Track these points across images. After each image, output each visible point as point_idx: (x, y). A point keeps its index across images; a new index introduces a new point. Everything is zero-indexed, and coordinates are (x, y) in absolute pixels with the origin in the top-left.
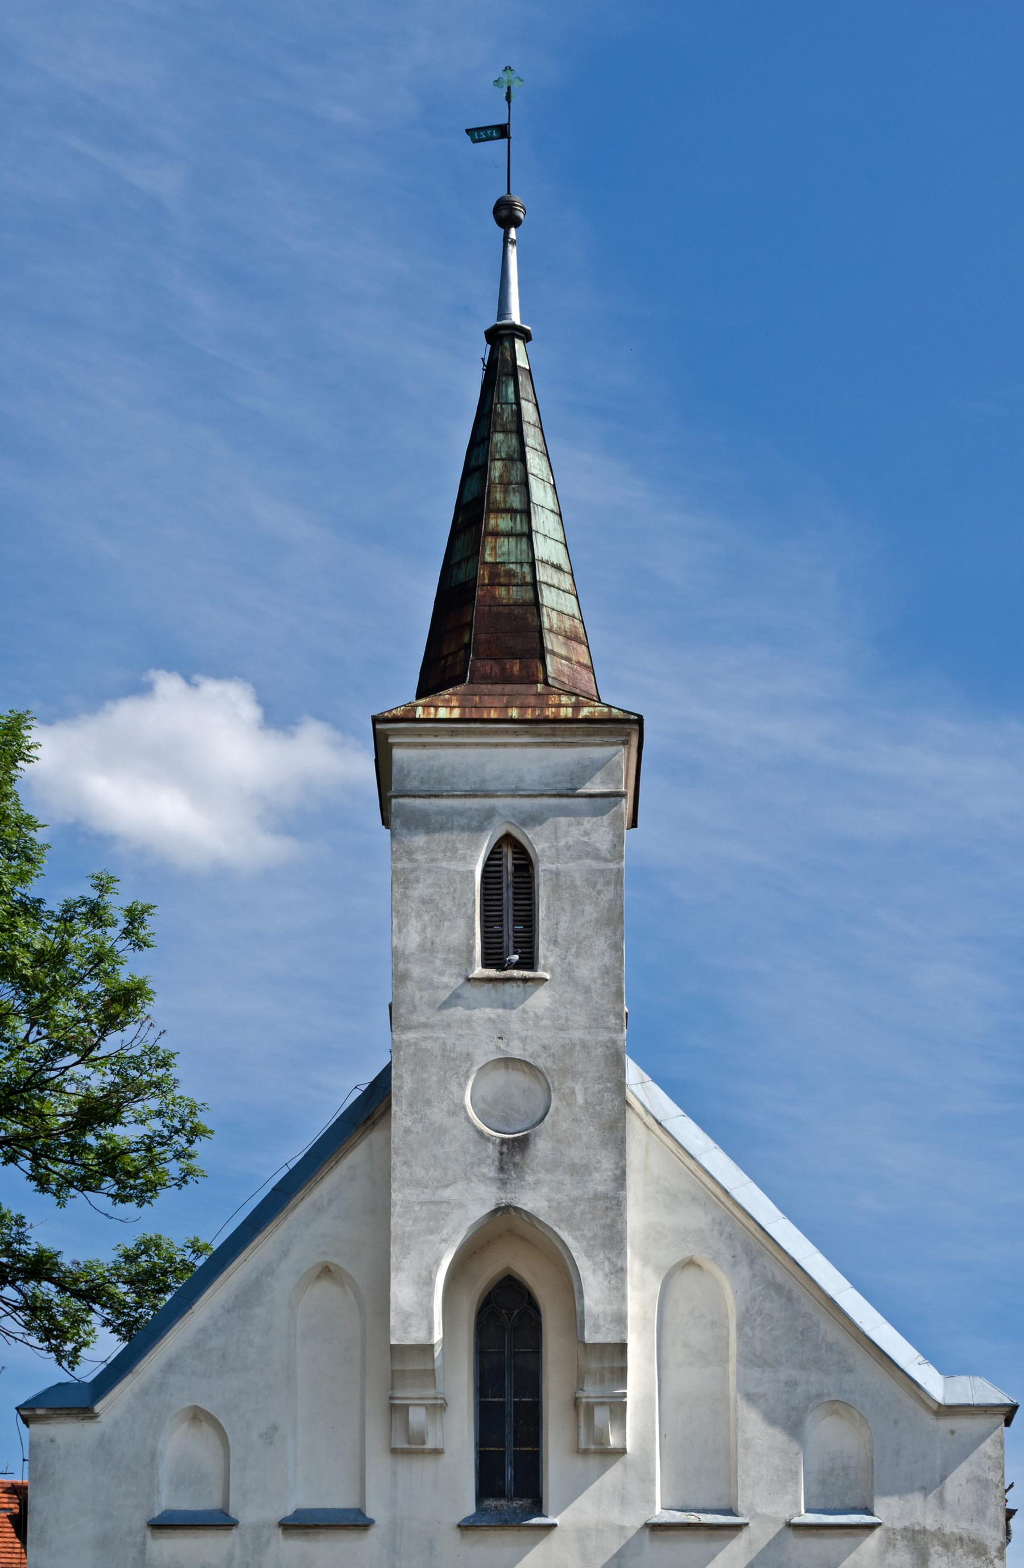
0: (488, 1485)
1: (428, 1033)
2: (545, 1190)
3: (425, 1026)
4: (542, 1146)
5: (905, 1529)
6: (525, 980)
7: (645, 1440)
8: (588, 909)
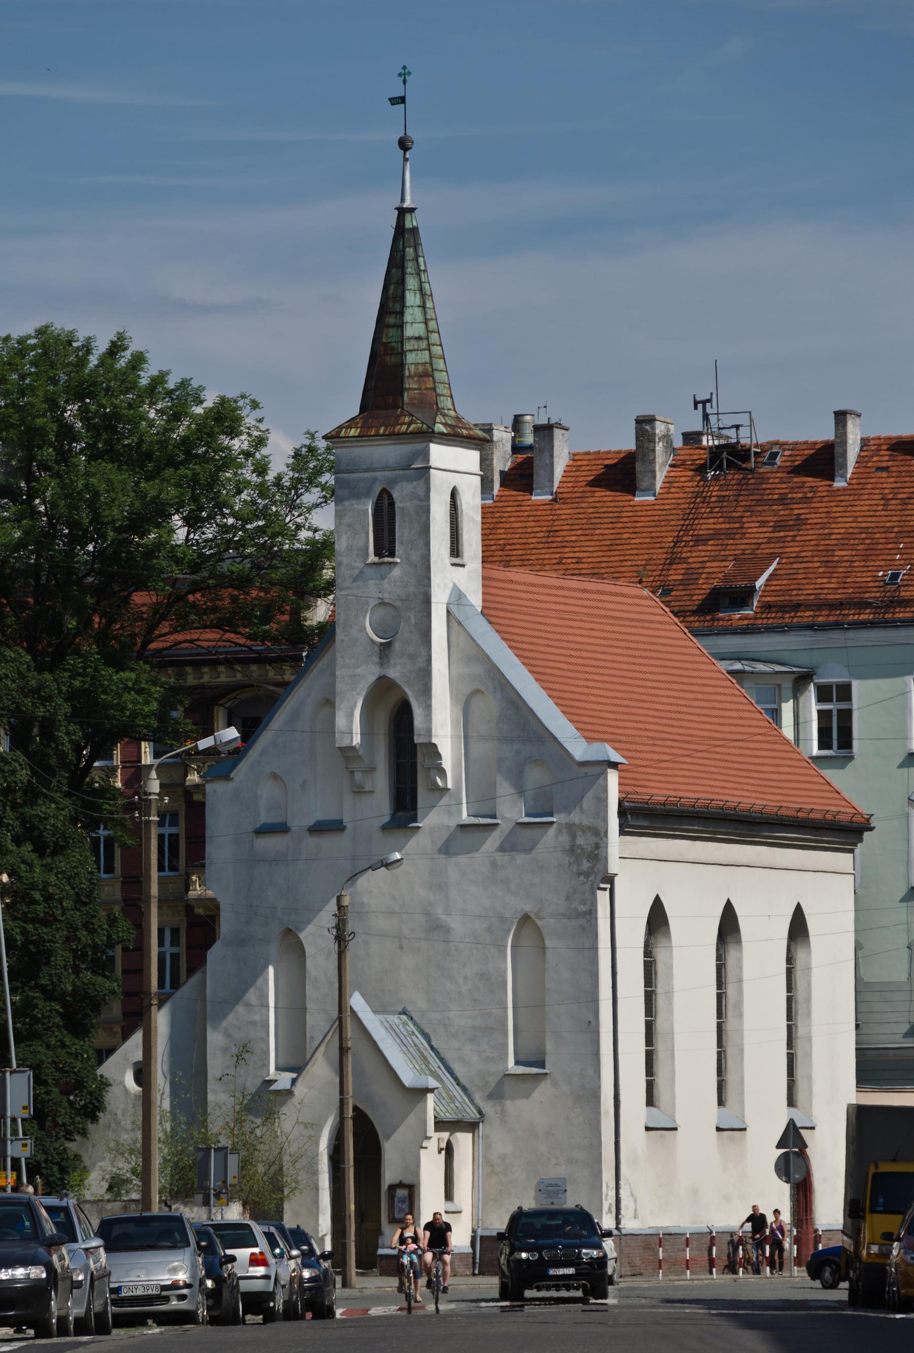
2: (399, 667)
3: (349, 588)
4: (397, 646)
5: (566, 824)
6: (390, 563)
7: (457, 783)
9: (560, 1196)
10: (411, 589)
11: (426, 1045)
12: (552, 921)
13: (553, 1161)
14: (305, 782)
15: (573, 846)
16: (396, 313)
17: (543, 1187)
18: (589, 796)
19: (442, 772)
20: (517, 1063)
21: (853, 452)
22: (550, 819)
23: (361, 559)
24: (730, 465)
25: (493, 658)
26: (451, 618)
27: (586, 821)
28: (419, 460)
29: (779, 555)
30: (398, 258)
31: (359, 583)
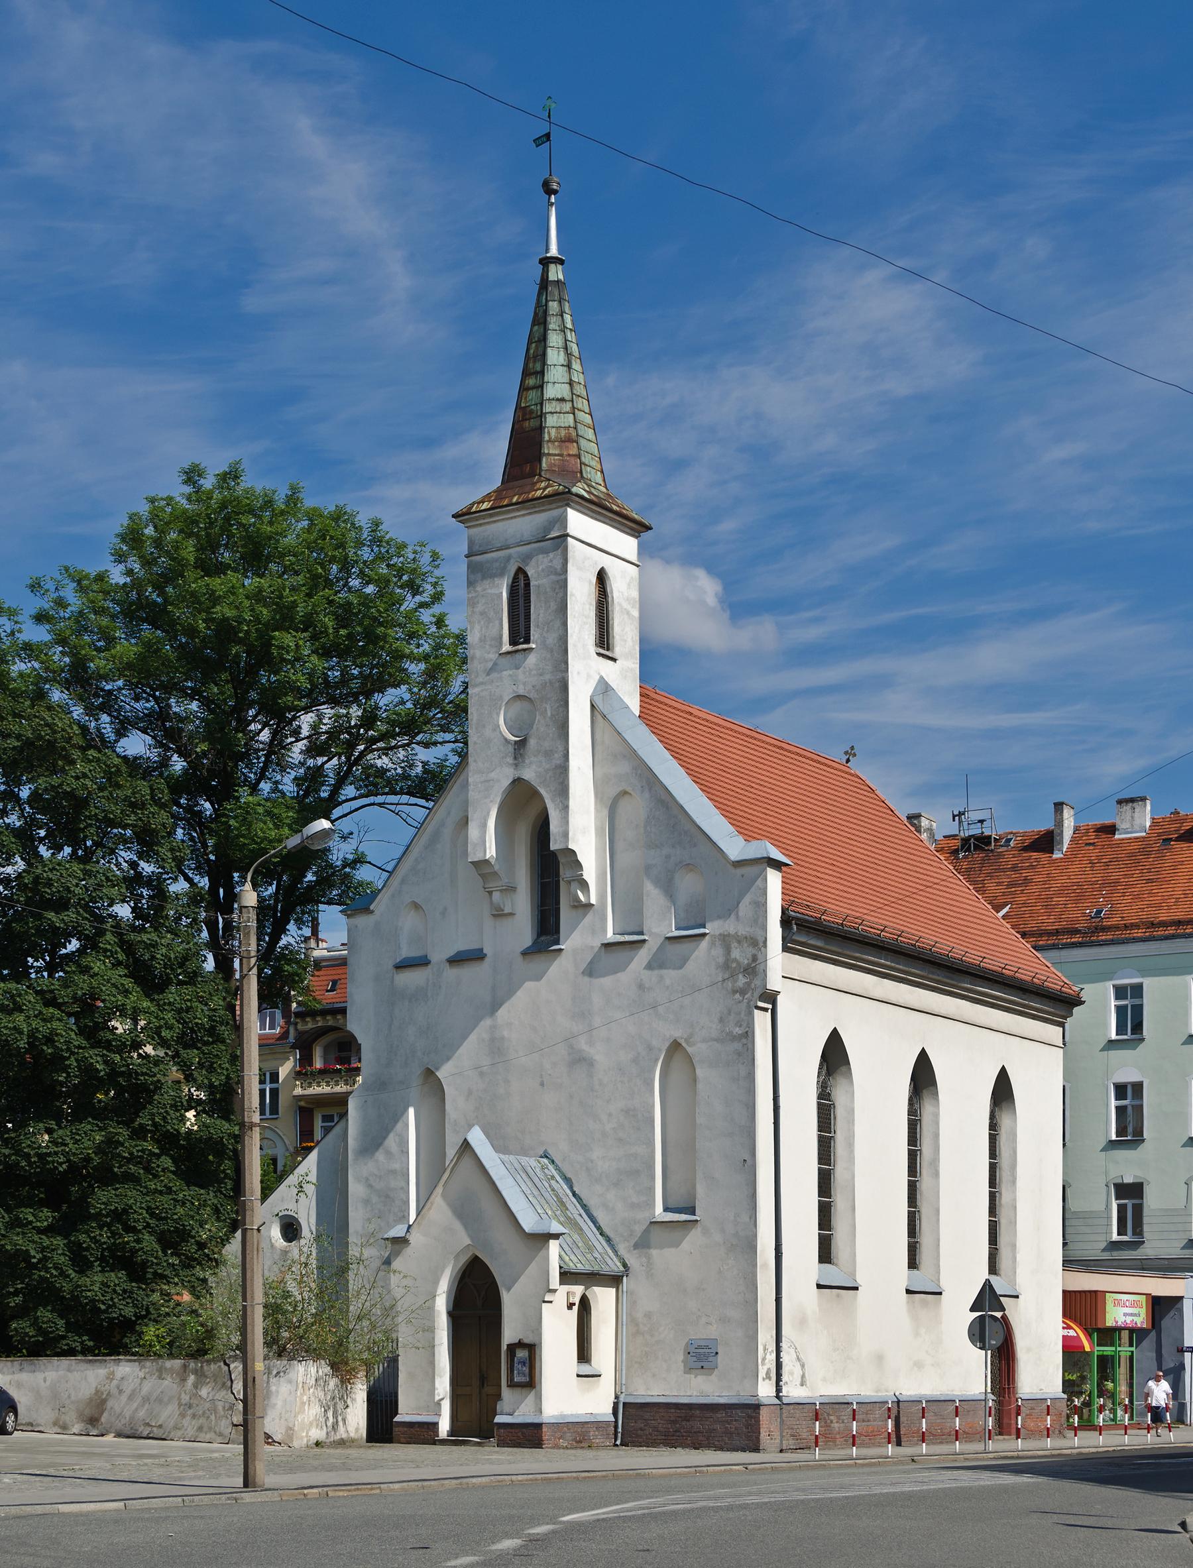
1: (483, 687)
2: (534, 767)
3: (482, 683)
4: (532, 742)
6: (525, 650)
9: (711, 1359)
10: (548, 677)
11: (568, 1192)
12: (703, 1046)
13: (704, 1320)
15: (727, 960)
16: (536, 373)
17: (692, 1350)
18: (747, 900)
19: (584, 885)
20: (666, 1209)
21: (1068, 834)
22: (702, 931)
23: (494, 650)
24: (977, 847)
25: (640, 752)
26: (599, 718)
27: (743, 930)
29: (1011, 903)
30: (540, 314)
31: (494, 675)
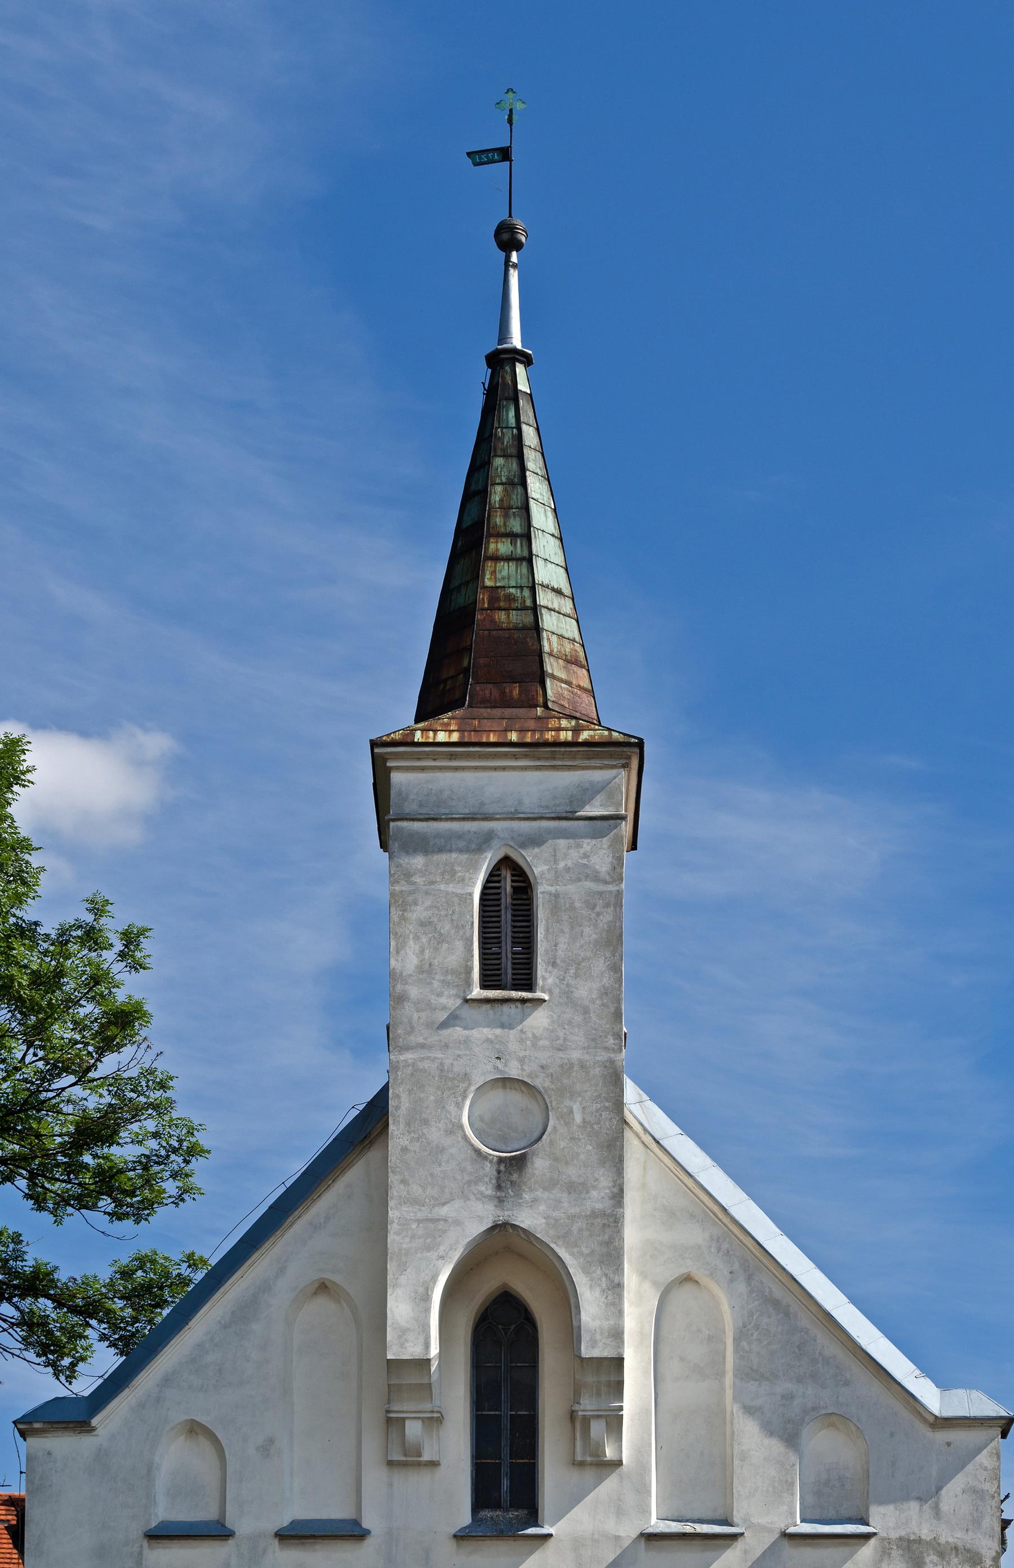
0: (484, 1495)
1: (425, 1053)
2: (542, 1208)
3: (423, 1046)
4: (539, 1165)
5: (901, 1539)
6: (523, 1001)
7: (641, 1452)
8: (587, 930)
14: (271, 1441)
28: (598, 799)
